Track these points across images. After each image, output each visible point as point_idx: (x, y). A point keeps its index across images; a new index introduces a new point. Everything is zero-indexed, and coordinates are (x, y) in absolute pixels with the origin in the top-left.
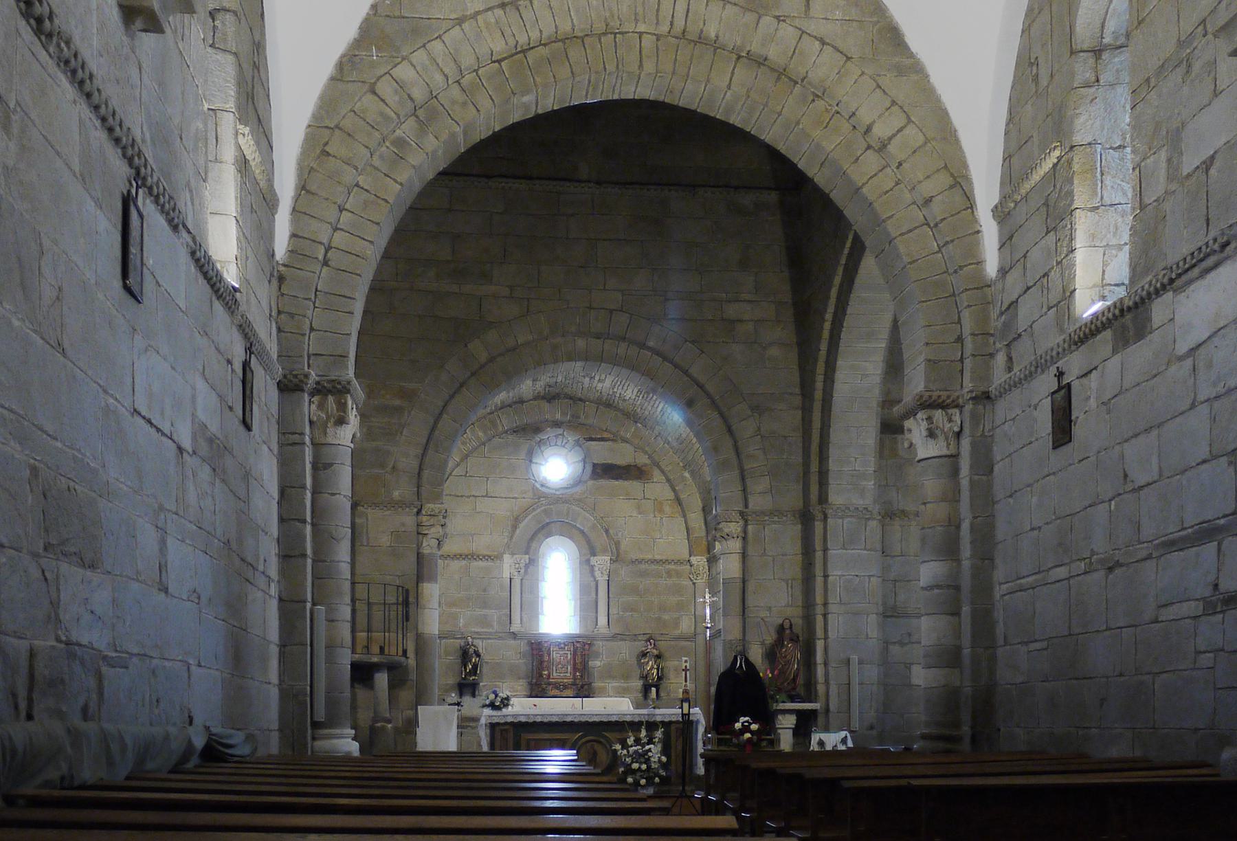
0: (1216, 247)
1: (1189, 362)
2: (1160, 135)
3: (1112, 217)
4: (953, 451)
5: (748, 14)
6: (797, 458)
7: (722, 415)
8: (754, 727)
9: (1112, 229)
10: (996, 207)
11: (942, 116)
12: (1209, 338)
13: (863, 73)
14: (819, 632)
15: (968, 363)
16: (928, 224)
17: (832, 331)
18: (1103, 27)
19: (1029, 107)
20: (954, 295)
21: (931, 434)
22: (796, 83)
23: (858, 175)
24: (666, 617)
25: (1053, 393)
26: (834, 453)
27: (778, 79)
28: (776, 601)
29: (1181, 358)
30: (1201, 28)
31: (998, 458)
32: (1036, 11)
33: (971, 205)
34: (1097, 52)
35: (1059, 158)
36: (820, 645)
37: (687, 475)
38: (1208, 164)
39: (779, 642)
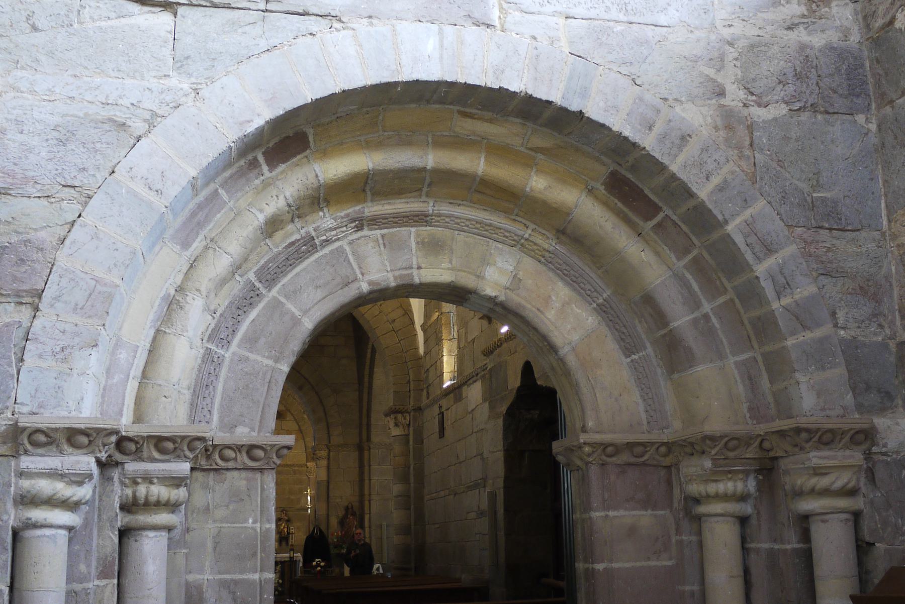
4: (406, 433)
8: (322, 564)
14: (367, 510)
21: (396, 425)
24: (292, 497)
28: (344, 493)
33: (412, 323)
36: (367, 517)
38: (473, 340)
39: (345, 517)
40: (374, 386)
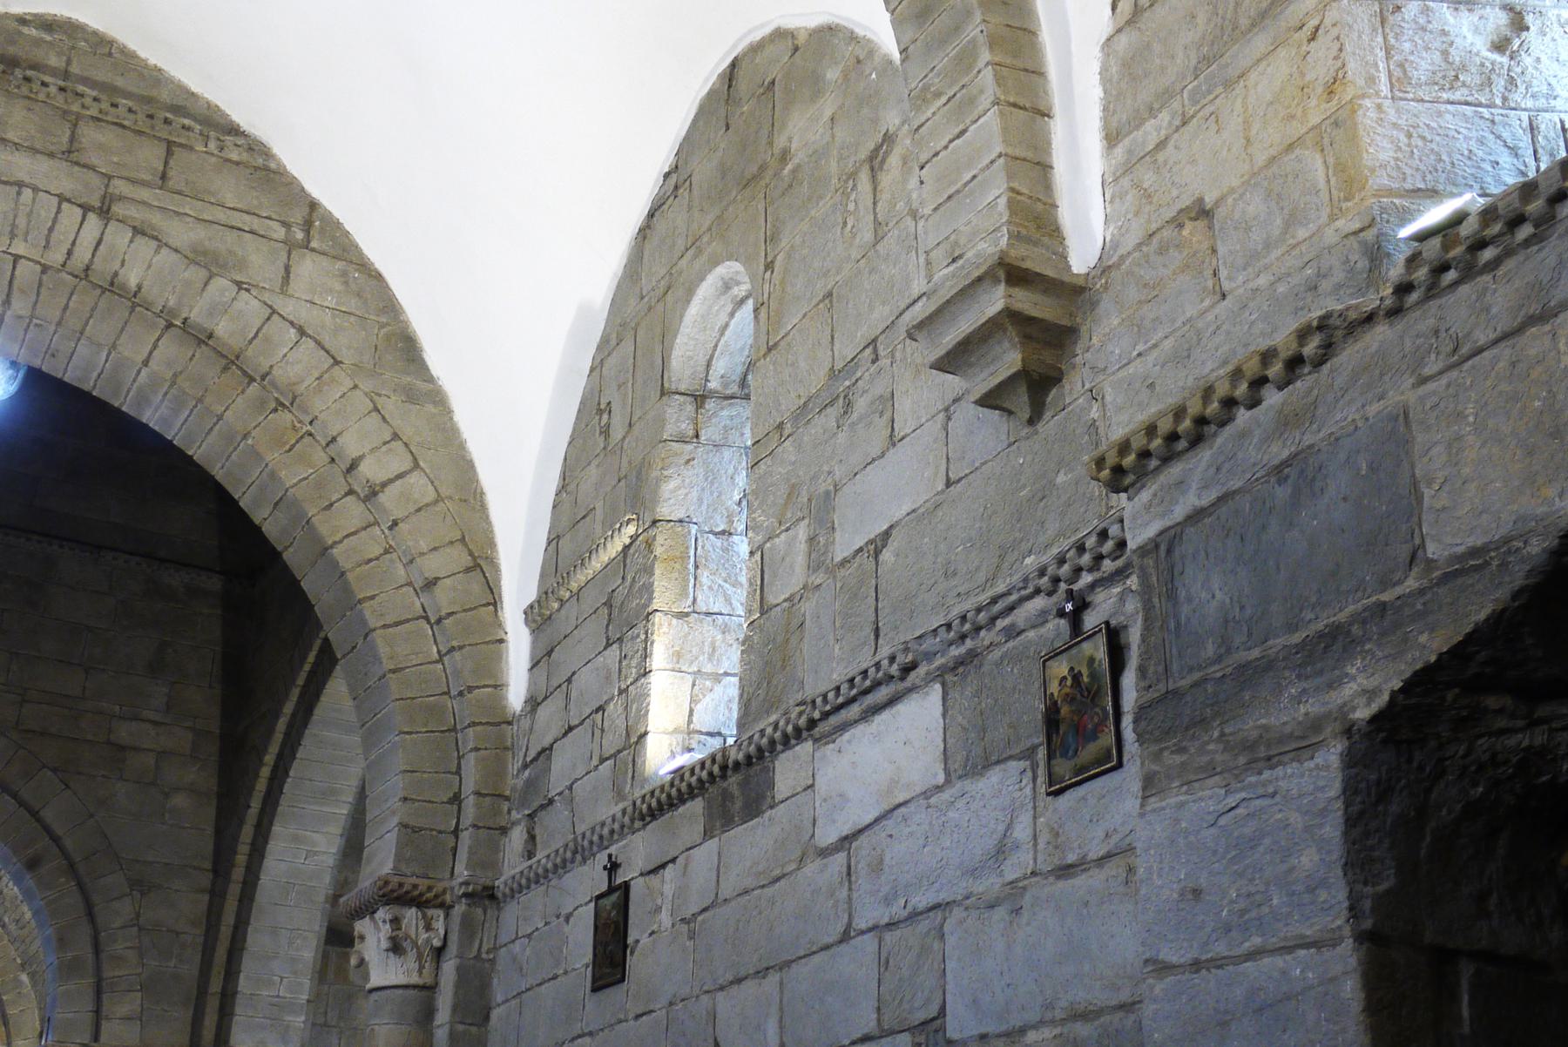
0: (894, 670)
1: (841, 858)
2: (796, 503)
3: (707, 631)
4: (427, 979)
5: (193, 268)
6: (190, 970)
7: (81, 886)
9: (707, 649)
10: (531, 606)
11: (466, 468)
12: (877, 820)
13: (356, 387)
15: (466, 837)
16: (427, 619)
17: (272, 779)
18: (708, 365)
19: (593, 471)
20: (454, 729)
21: (396, 948)
22: (252, 380)
23: (326, 528)
25: (599, 897)
26: (248, 967)
27: (225, 369)
29: (824, 853)
30: (868, 351)
31: (499, 999)
32: (613, 343)
33: (495, 603)
34: (699, 399)
35: (634, 538)
37: (24, 978)
38: (878, 544)
40: (265, 880)
